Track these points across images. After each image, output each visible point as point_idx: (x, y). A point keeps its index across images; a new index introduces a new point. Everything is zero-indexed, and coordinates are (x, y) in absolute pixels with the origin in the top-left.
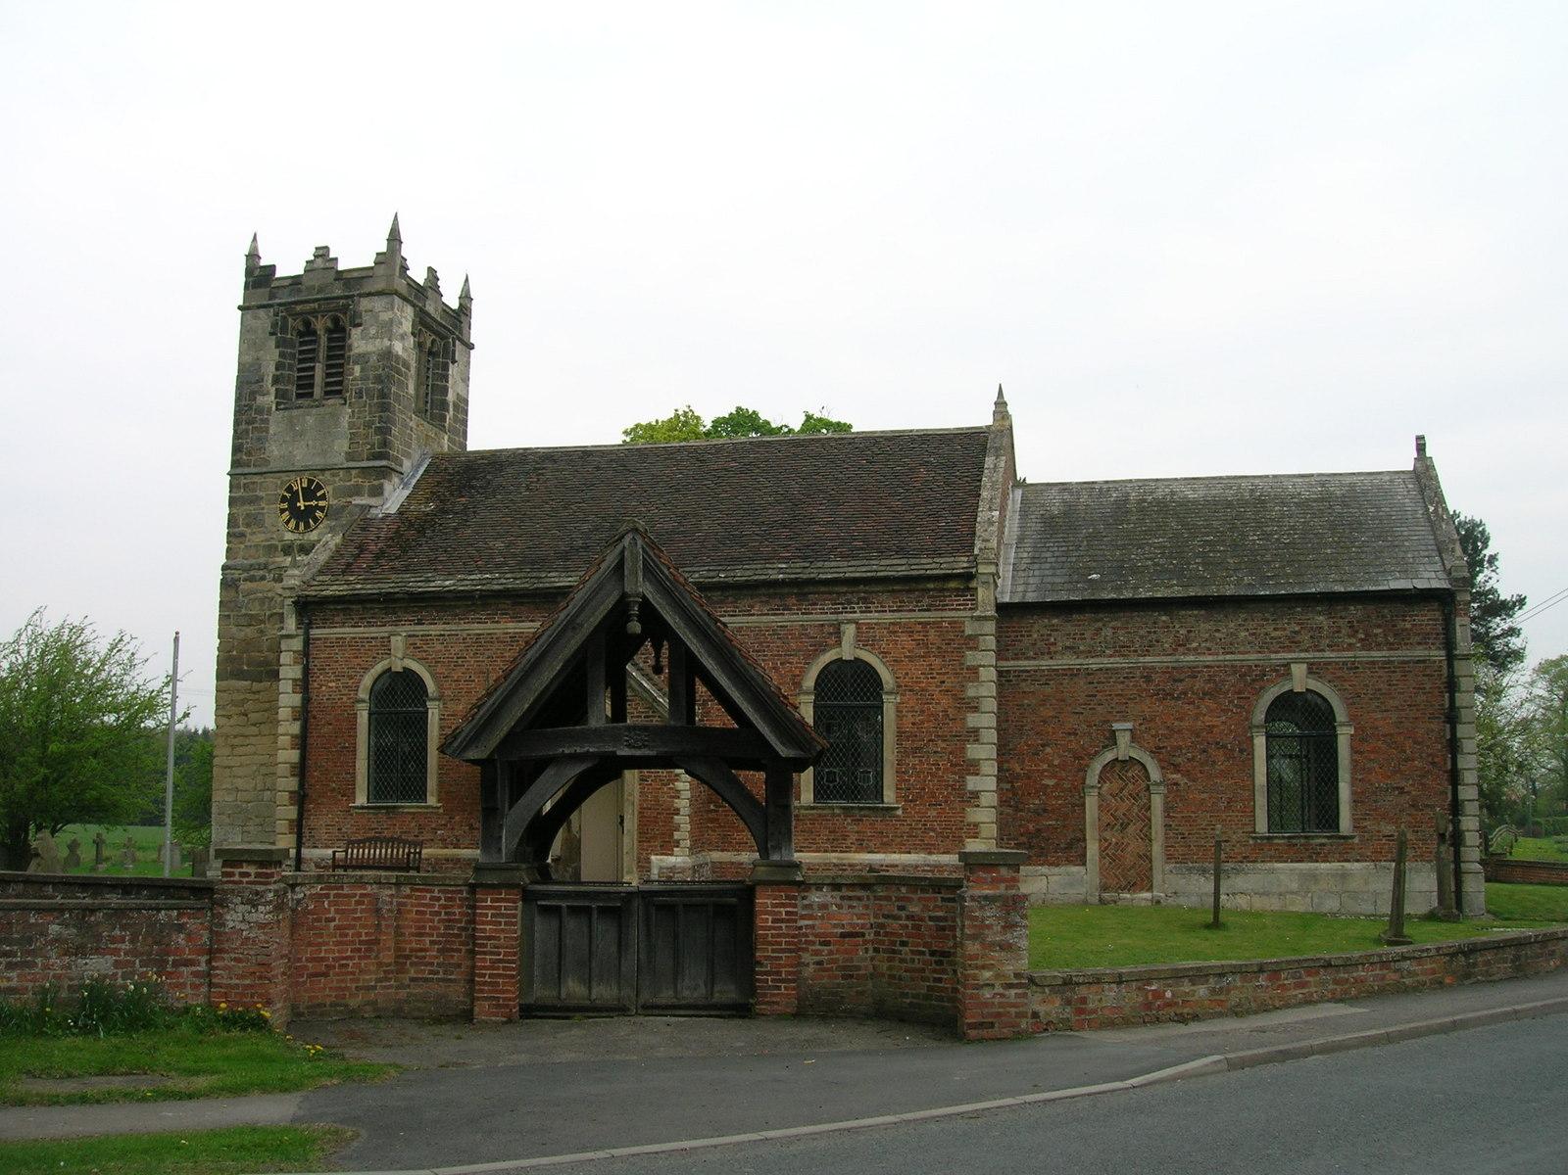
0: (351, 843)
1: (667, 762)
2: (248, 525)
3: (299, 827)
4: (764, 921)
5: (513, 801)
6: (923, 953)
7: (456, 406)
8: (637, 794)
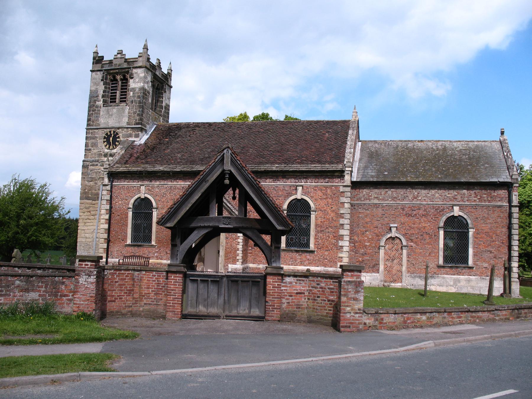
0: (125, 257)
1: (236, 230)
2: (92, 146)
3: (107, 250)
4: (269, 287)
5: (181, 244)
6: (325, 300)
7: (165, 108)
8: (224, 243)
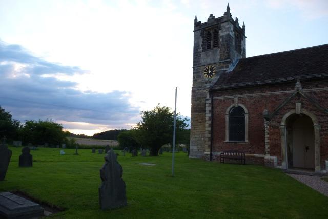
0: (225, 152)
